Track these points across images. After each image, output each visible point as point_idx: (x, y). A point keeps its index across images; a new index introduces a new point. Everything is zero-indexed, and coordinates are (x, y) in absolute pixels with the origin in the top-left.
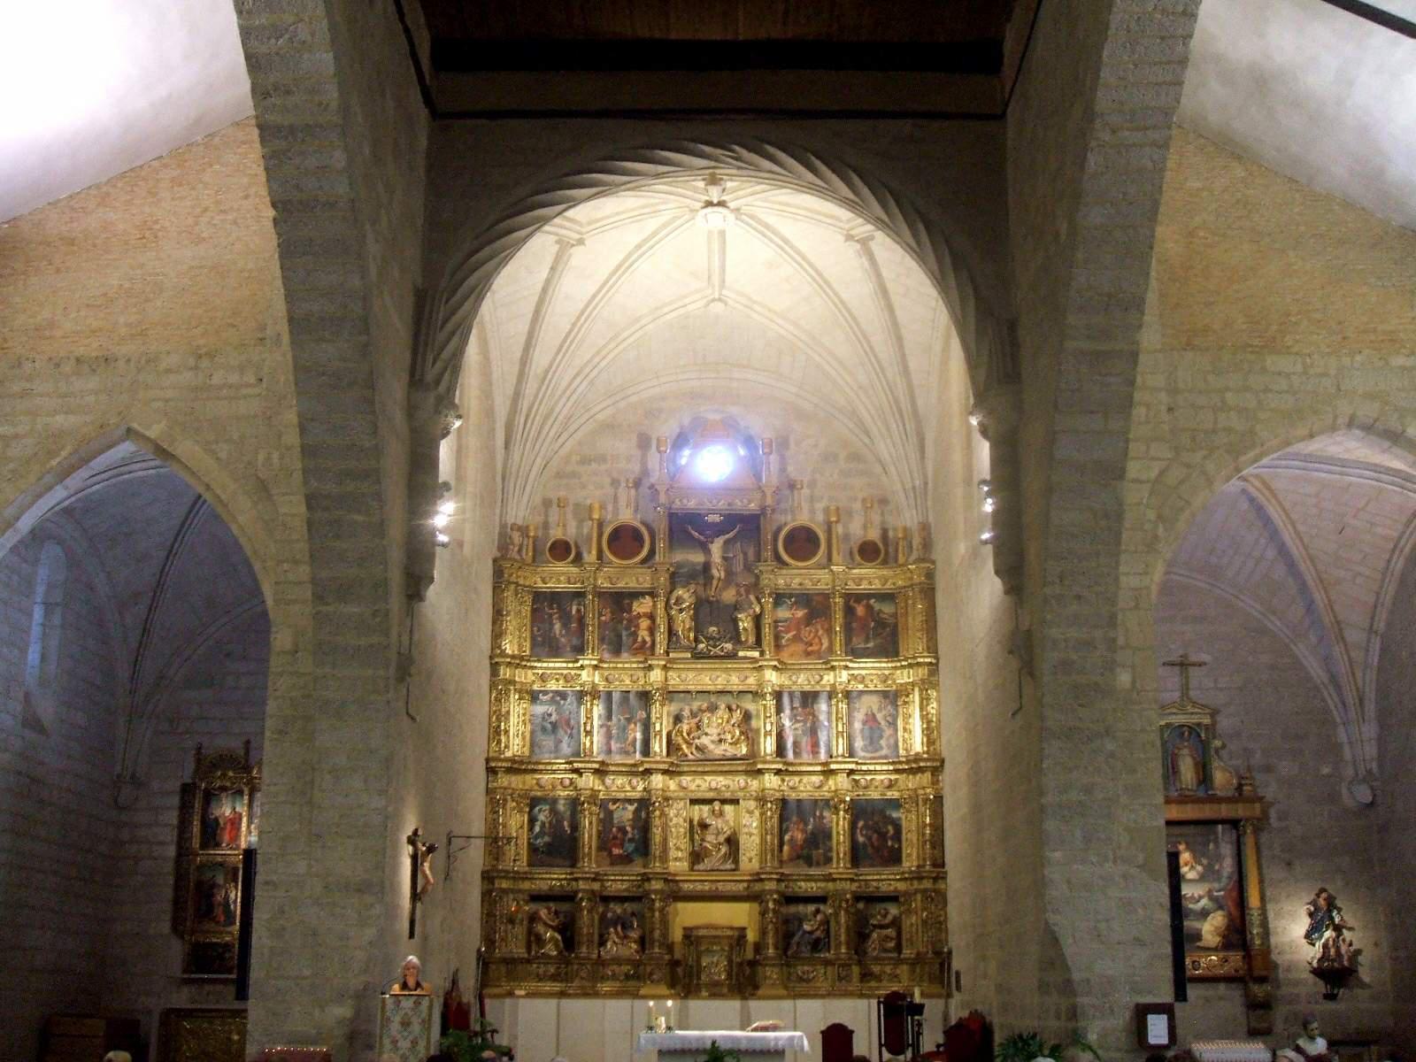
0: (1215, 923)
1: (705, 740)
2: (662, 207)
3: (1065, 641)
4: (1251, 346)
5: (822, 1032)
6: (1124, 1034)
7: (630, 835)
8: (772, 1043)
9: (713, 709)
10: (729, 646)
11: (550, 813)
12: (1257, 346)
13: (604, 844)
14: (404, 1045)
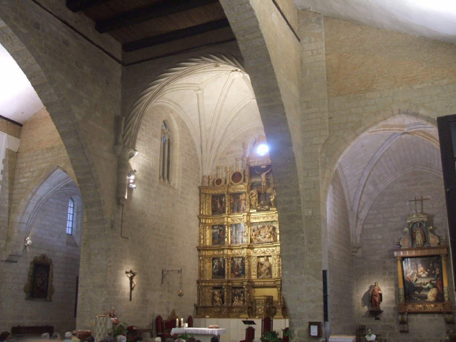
0: (433, 292)
1: (260, 237)
2: (221, 75)
3: (283, 201)
4: (361, 91)
5: (246, 329)
6: (306, 332)
7: (240, 268)
8: (207, 332)
9: (263, 227)
10: (267, 207)
11: (218, 262)
12: (363, 90)
13: (233, 271)
14: (100, 330)
